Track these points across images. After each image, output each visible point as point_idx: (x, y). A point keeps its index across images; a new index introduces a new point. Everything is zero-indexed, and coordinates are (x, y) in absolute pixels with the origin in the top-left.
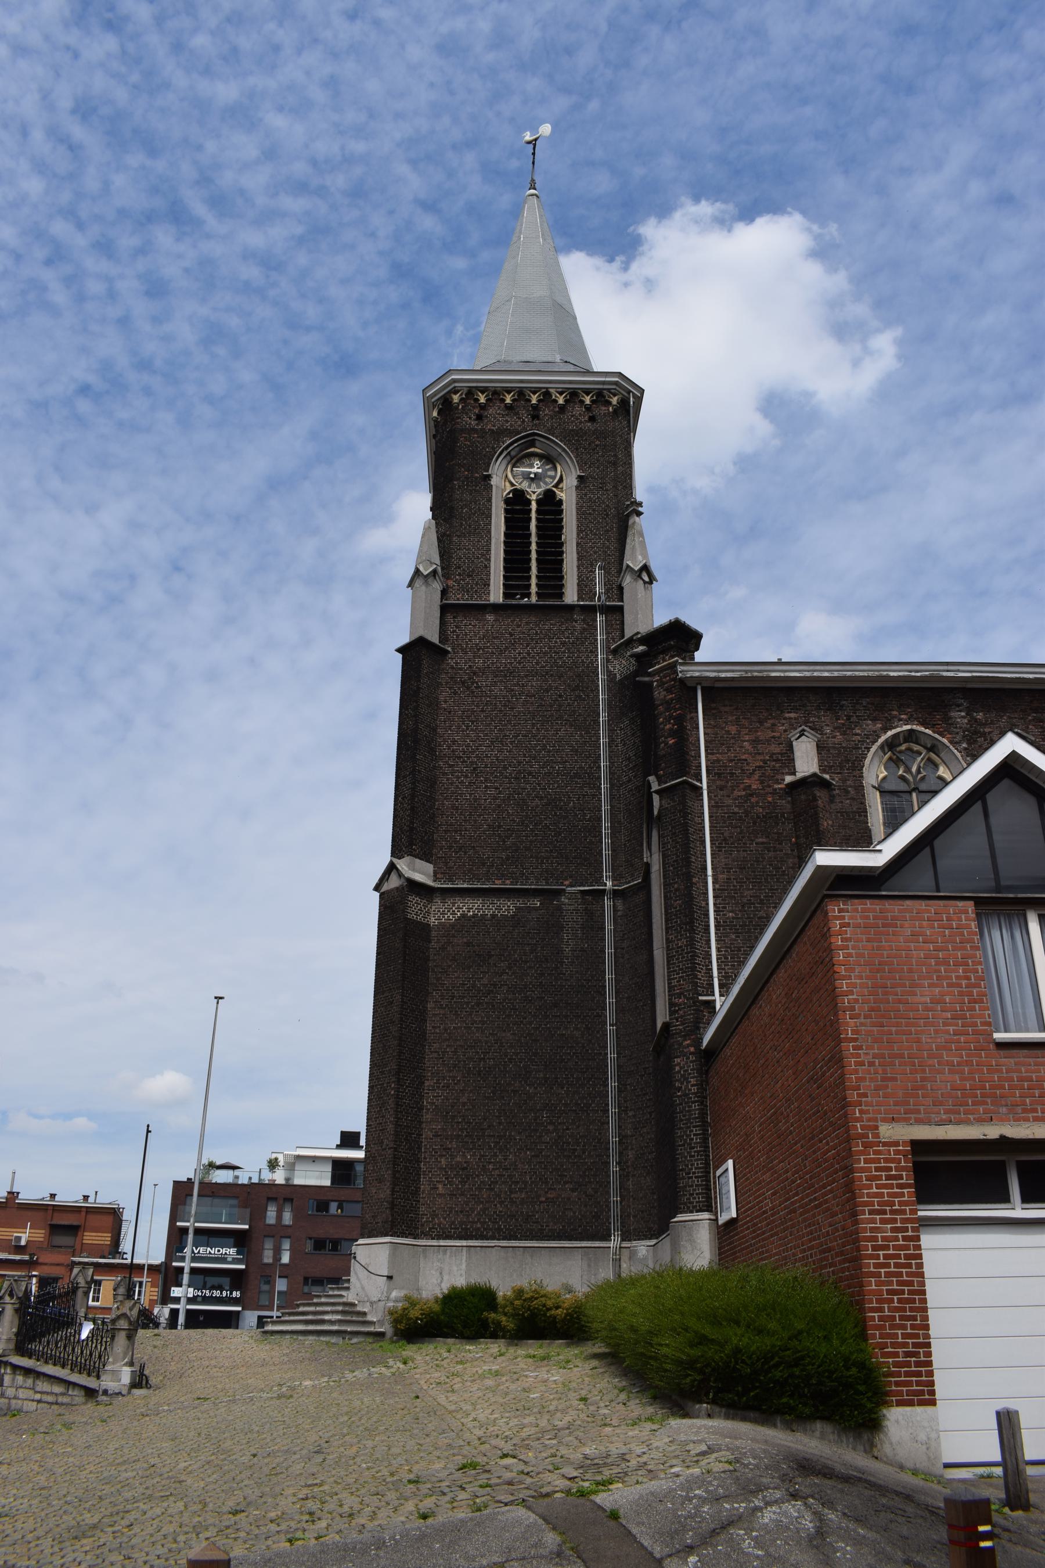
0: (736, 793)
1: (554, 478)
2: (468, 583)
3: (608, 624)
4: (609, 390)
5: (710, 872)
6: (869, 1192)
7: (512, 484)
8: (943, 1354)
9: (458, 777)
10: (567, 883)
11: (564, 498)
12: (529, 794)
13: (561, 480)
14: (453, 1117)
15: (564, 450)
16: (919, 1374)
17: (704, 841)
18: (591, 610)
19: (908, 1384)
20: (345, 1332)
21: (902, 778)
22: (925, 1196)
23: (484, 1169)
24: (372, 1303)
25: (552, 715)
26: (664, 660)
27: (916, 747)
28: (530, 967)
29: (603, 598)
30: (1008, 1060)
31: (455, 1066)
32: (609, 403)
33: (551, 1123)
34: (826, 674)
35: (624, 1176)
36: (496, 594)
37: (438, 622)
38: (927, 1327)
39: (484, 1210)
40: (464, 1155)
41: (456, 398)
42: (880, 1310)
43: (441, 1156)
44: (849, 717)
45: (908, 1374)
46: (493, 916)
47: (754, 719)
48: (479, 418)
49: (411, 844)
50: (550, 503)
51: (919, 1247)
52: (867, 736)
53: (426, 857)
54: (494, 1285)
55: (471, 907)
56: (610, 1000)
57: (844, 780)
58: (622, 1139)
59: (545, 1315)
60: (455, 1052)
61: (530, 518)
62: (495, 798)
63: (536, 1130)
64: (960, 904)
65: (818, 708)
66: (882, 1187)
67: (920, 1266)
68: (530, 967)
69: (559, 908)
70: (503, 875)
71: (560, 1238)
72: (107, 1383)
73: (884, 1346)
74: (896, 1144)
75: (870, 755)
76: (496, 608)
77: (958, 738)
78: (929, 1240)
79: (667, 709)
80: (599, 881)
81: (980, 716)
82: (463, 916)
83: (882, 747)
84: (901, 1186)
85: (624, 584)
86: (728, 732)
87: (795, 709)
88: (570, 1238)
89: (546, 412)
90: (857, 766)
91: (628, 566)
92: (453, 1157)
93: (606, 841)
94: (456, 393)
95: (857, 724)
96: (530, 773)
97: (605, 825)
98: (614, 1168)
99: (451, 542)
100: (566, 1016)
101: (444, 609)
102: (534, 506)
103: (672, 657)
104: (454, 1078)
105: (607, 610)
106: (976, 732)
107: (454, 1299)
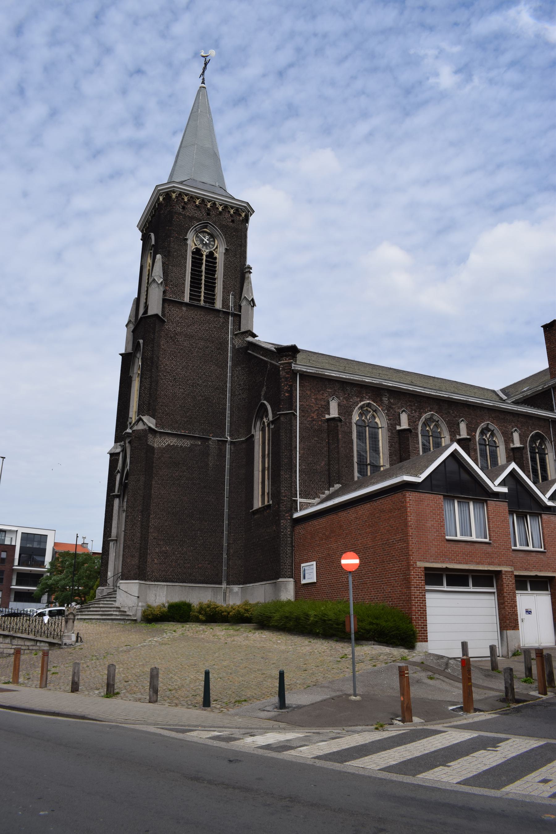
0: (308, 419)
1: (214, 245)
2: (175, 290)
3: (234, 322)
4: (241, 209)
5: (298, 450)
6: (414, 582)
7: (196, 245)
9: (168, 382)
10: (211, 435)
11: (218, 257)
12: (197, 394)
13: (217, 248)
14: (162, 531)
15: (220, 234)
16: (424, 633)
17: (296, 437)
18: (228, 313)
19: (421, 636)
20: (125, 619)
21: (364, 421)
22: (427, 583)
23: (174, 553)
24: (129, 608)
25: (208, 360)
26: (286, 360)
27: (369, 409)
28: (195, 470)
29: (233, 309)
30: (449, 545)
31: (163, 510)
32: (241, 215)
33: (201, 536)
34: (344, 377)
35: (228, 559)
36: (187, 299)
37: (161, 306)
38: (426, 620)
40: (166, 548)
41: (174, 196)
42: (415, 615)
43: (156, 547)
44: (349, 395)
45: (422, 633)
46: (181, 446)
47: (316, 390)
48: (184, 208)
49: (149, 410)
50: (211, 255)
51: (425, 598)
52: (354, 403)
53: (153, 416)
54: (191, 602)
55: (172, 441)
56: (227, 487)
57: (346, 419)
58: (229, 544)
59: (221, 614)
61: (202, 263)
62: (183, 394)
63: (195, 539)
64: (440, 496)
65: (339, 389)
66: (417, 579)
67: (425, 603)
68: (195, 470)
69: (208, 446)
70: (185, 429)
72: (66, 640)
73: (416, 625)
74: (421, 568)
75: (355, 411)
76: (186, 304)
77: (384, 408)
78: (428, 596)
79: (286, 381)
80: (224, 436)
82: (169, 445)
83: (359, 408)
84: (421, 580)
85: (242, 305)
86: (307, 394)
87: (331, 388)
88: (207, 583)
89: (213, 213)
90: (350, 414)
91: (245, 297)
93: (228, 419)
94: (174, 192)
95: (351, 398)
96: (198, 385)
97: (228, 412)
98: (225, 556)
99: (168, 268)
100: (209, 492)
101: (164, 301)
102: (204, 257)
103: (290, 359)
105: (234, 315)
106: (390, 407)
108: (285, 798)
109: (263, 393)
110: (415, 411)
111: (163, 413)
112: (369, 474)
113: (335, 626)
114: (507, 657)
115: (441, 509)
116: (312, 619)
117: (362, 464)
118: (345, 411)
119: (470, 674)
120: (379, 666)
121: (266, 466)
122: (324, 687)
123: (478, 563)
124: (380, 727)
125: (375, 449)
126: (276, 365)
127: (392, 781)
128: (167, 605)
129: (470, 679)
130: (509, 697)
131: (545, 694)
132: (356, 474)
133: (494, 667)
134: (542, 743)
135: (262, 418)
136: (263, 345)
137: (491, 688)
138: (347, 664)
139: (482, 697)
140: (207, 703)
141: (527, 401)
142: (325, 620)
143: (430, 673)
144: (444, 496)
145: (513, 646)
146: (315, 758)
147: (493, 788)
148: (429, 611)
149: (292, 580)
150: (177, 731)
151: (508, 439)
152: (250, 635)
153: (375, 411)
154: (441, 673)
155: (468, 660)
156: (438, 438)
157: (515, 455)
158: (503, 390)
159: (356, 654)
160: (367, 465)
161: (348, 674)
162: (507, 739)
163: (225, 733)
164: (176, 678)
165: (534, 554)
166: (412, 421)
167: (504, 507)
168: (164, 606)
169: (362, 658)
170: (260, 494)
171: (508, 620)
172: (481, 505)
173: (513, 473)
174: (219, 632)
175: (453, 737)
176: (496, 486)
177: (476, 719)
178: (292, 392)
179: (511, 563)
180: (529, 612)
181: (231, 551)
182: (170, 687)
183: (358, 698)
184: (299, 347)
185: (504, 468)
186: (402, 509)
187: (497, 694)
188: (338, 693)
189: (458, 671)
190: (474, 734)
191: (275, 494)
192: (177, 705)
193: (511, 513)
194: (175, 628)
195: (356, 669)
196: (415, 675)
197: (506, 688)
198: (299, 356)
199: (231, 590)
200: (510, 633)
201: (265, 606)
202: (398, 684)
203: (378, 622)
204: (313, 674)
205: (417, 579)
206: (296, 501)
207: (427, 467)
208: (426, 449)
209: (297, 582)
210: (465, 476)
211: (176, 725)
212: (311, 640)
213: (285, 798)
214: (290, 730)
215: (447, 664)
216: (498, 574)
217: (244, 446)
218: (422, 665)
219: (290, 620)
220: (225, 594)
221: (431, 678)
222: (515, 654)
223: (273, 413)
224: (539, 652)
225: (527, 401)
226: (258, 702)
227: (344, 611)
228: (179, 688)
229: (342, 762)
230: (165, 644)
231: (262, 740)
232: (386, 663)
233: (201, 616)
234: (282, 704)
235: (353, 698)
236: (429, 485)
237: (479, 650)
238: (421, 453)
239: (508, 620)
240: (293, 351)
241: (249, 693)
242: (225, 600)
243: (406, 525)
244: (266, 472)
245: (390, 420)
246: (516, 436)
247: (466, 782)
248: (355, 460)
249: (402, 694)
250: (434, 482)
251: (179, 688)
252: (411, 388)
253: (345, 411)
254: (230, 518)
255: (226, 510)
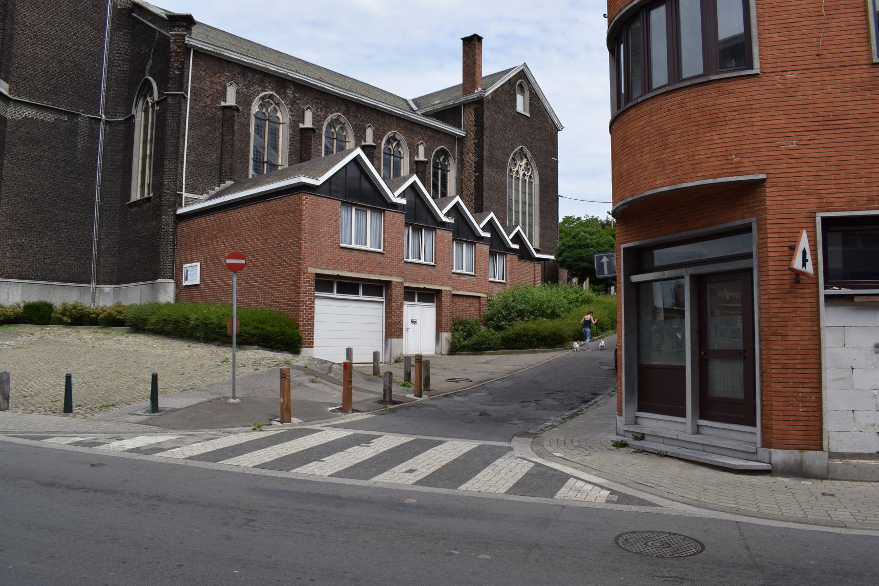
8: (317, 334)
21: (264, 113)
22: (317, 290)
30: (343, 252)
35: (99, 256)
39: (30, 266)
46: (42, 120)
54: (52, 302)
55: (31, 113)
56: (99, 174)
60: (18, 188)
66: (307, 284)
69: (77, 123)
71: (67, 281)
78: (317, 302)
79: (177, 56)
80: (97, 113)
81: (297, 95)
82: (26, 117)
87: (229, 72)
88: (72, 282)
90: (249, 105)
92: (15, 240)
93: (103, 94)
97: (103, 85)
98: (94, 252)
104: (17, 201)
107: (29, 307)
108: (152, 497)
109: (148, 67)
110: (322, 110)
111: (19, 77)
112: (265, 172)
113: (217, 330)
114: (389, 363)
115: (338, 215)
116: (192, 322)
117: (259, 162)
118: (244, 100)
119: (351, 377)
120: (261, 369)
121: (148, 153)
122: (202, 390)
123: (370, 273)
124: (258, 428)
125: (274, 146)
126: (166, 36)
127: (265, 477)
128: (22, 305)
129: (350, 382)
130: (387, 399)
131: (420, 396)
132: (251, 172)
133: (376, 372)
134: (412, 438)
135: (145, 97)
136: (152, 9)
137: (368, 391)
138: (228, 367)
139: (362, 399)
140: (68, 408)
141: (438, 115)
142: (206, 324)
143: (312, 377)
144: (342, 202)
145: (396, 353)
146: (187, 459)
147: (363, 479)
148: (317, 318)
149: (172, 281)
150: (32, 438)
151: (414, 152)
152: (123, 338)
153: (277, 104)
154: (323, 377)
155: (351, 364)
156: (342, 141)
157: (418, 168)
158: (415, 101)
159: (237, 358)
160: (264, 163)
161: (229, 378)
162: (381, 436)
163: (89, 438)
164: (32, 383)
165: (424, 267)
166: (317, 120)
167: (401, 218)
168: (19, 306)
169: (243, 362)
170: (139, 184)
171: (393, 328)
172: (379, 215)
173: (413, 186)
174: (87, 334)
175: (330, 435)
176: (395, 197)
177: (353, 419)
178: (183, 69)
179: (402, 275)
180: (414, 322)
181: (103, 247)
182: (24, 393)
183: (237, 401)
184: (196, 18)
185: (406, 179)
186: (297, 212)
187: (376, 396)
188: (216, 396)
189: (339, 374)
190: (350, 432)
191: (157, 186)
192: (32, 412)
193: (407, 225)
194: (32, 331)
195: (237, 373)
196: (297, 379)
197: (385, 390)
198: (194, 29)
199: (101, 291)
200: (394, 341)
201: (140, 308)
202: (279, 387)
203: (263, 326)
204: (190, 378)
205: (307, 284)
206: (181, 196)
207: (327, 170)
208: (328, 151)
209: (178, 284)
210: (366, 185)
211: (31, 432)
212: (191, 344)
213: (152, 497)
214: (162, 433)
215: (330, 369)
216: (388, 284)
217: (122, 127)
218: (305, 369)
219: (169, 323)
220: (94, 294)
221: (313, 382)
222: (396, 362)
223: (159, 93)
224: (419, 358)
225: (438, 115)
226: (128, 406)
227: (228, 315)
228: (36, 394)
229: (215, 461)
230: (20, 348)
231: (129, 443)
232: (269, 367)
233: (65, 319)
234: (155, 408)
235: (232, 400)
236: (329, 189)
237: (362, 357)
238: (323, 155)
239: (393, 328)
240: (187, 21)
241: (118, 398)
242: (94, 300)
243: (300, 229)
244: (148, 160)
245: (293, 116)
246: (421, 149)
247: (337, 475)
248: (251, 155)
249: (282, 396)
250: (333, 187)
251: (36, 394)
252: (319, 84)
253: (244, 100)
254: (102, 210)
255: (97, 200)
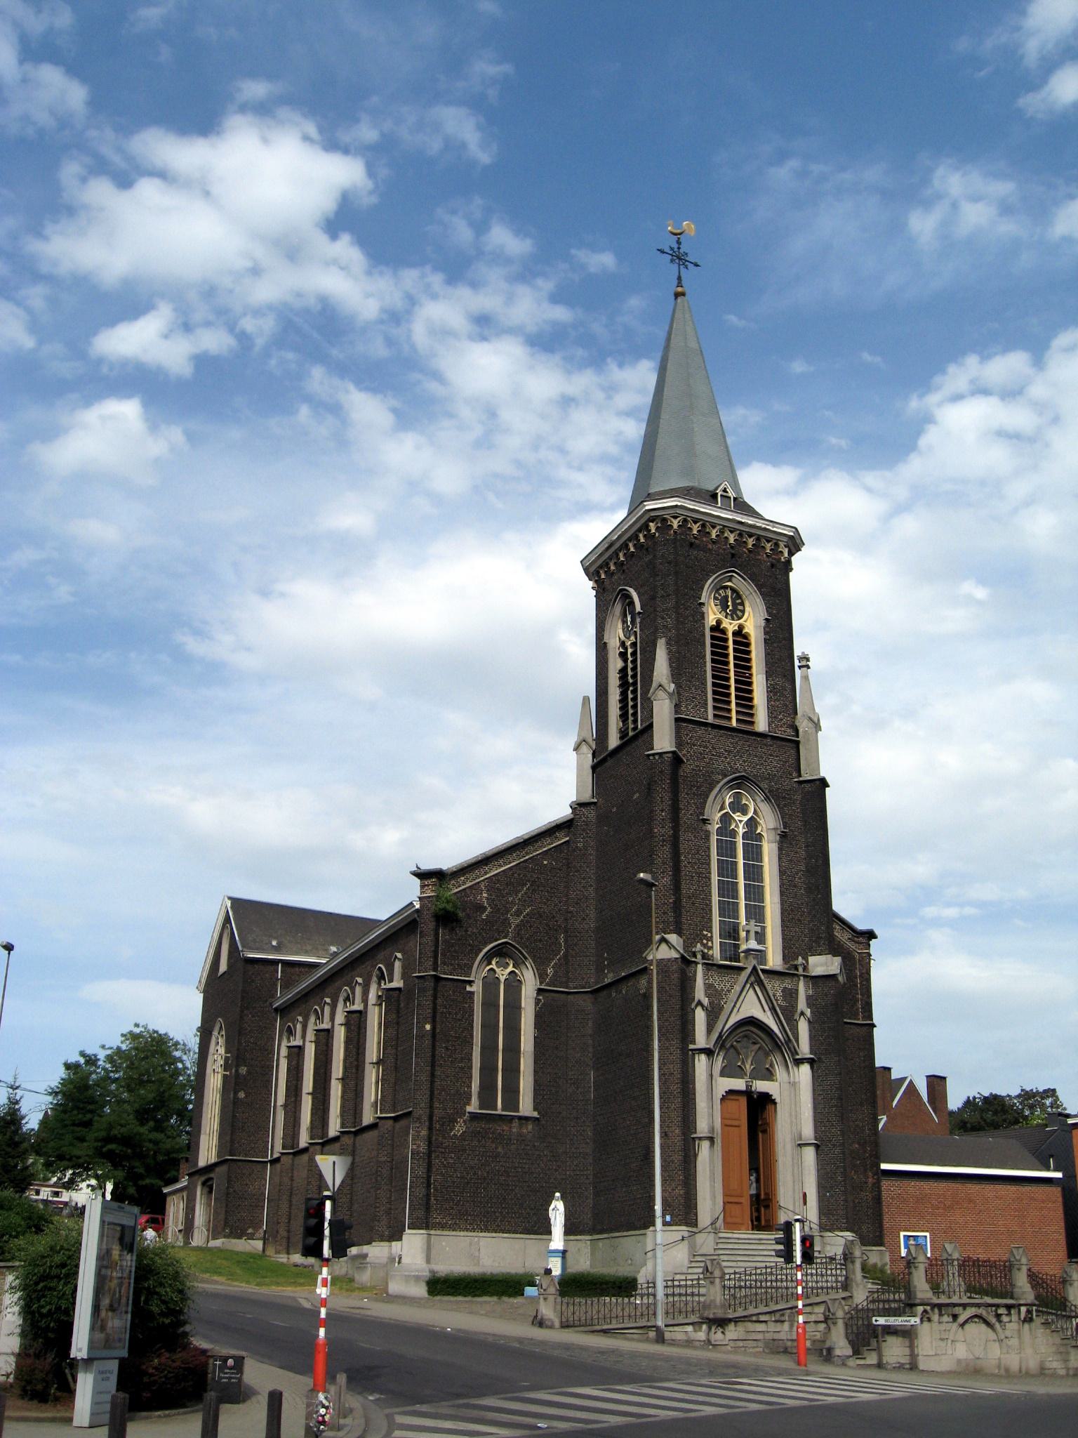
76: (713, 726)
